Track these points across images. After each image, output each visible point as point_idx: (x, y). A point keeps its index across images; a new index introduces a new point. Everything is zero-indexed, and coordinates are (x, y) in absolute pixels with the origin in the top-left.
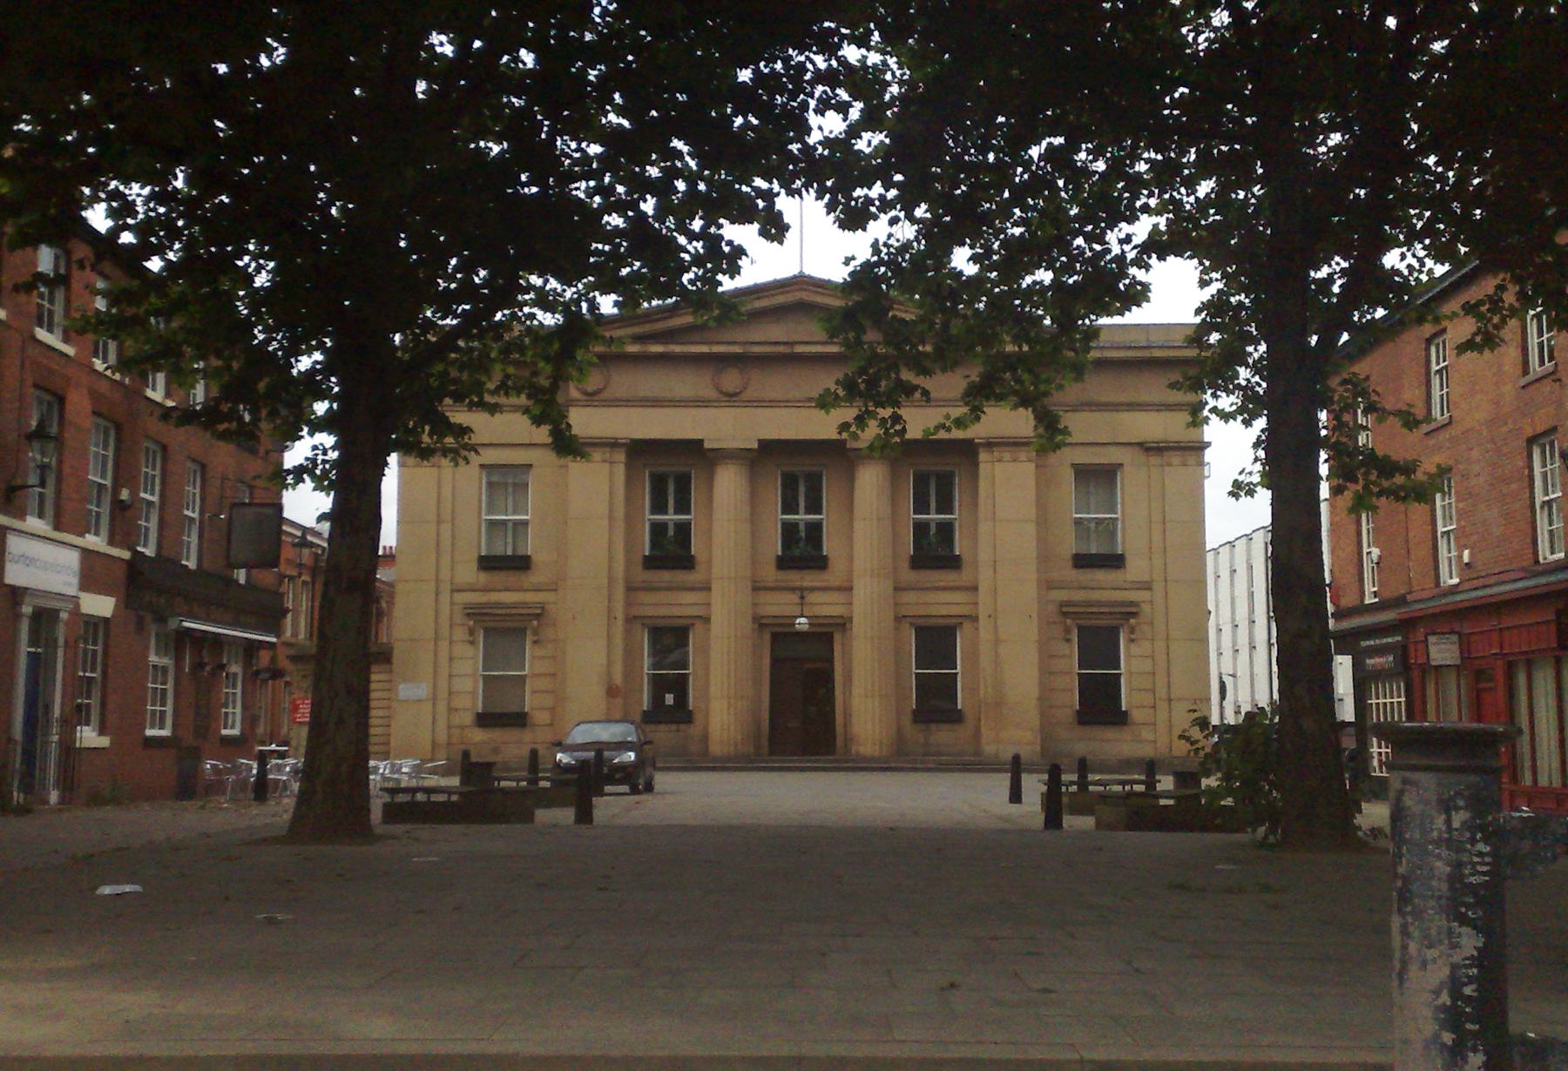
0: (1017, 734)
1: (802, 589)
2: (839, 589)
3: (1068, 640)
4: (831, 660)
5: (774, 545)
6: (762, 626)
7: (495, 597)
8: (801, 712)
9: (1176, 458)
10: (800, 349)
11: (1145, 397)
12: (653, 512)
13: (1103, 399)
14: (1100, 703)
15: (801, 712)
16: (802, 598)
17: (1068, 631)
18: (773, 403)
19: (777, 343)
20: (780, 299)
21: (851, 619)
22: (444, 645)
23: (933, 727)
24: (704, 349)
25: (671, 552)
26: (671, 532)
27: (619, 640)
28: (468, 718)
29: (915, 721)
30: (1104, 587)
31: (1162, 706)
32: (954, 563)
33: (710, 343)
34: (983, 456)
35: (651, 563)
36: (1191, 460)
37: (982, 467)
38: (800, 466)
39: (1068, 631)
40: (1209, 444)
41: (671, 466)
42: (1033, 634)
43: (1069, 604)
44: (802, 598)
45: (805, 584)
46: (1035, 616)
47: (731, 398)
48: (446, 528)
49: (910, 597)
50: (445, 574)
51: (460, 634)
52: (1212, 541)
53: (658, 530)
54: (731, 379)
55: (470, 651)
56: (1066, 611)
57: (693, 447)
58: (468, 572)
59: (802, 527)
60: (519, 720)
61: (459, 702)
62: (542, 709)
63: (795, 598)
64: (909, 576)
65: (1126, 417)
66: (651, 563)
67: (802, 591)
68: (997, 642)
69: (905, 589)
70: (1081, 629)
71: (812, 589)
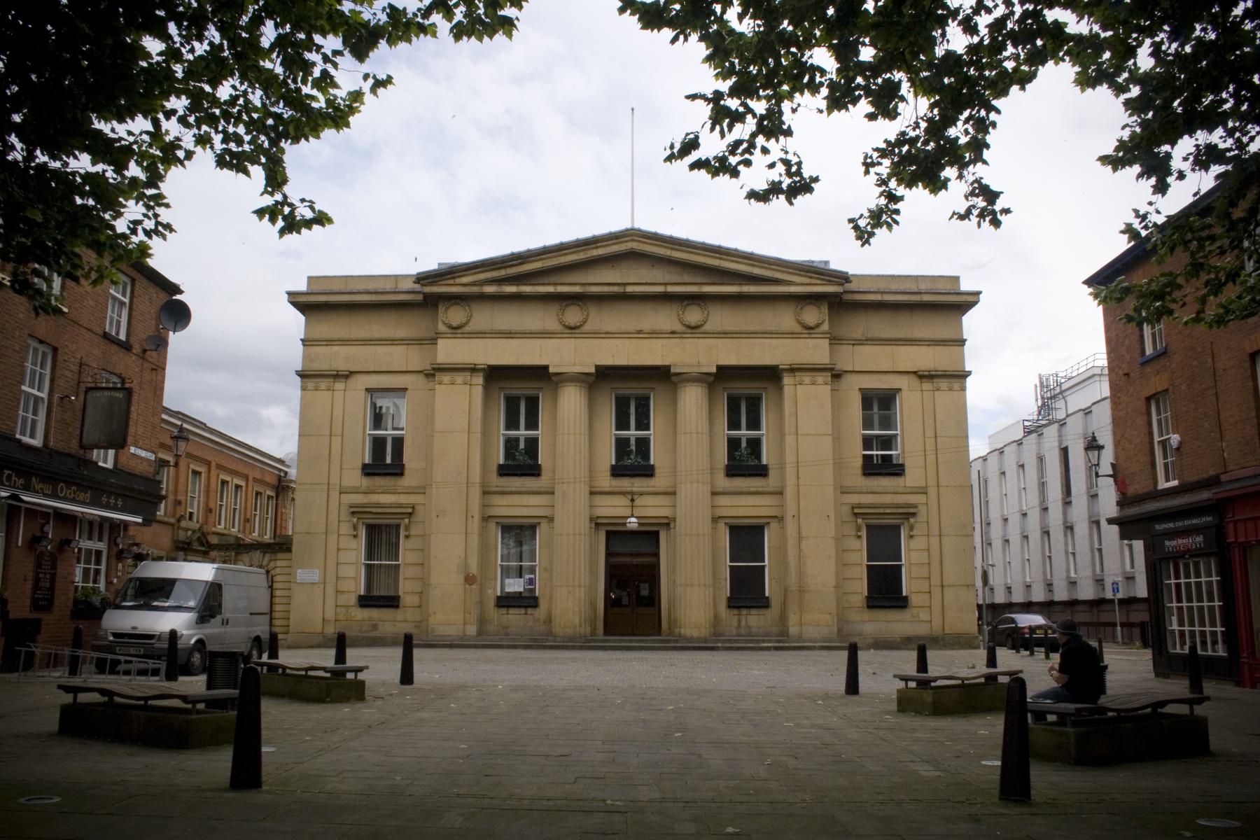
0: (815, 619)
1: (632, 493)
2: (665, 493)
3: (859, 537)
4: (657, 555)
5: (608, 456)
6: (597, 524)
7: (375, 498)
8: (632, 596)
9: (944, 384)
10: (630, 289)
11: (918, 333)
12: (617, 429)
13: (884, 336)
14: (885, 589)
15: (632, 596)
16: (632, 500)
17: (859, 529)
18: (608, 335)
19: (613, 284)
20: (616, 248)
21: (674, 519)
22: (333, 538)
23: (744, 612)
24: (550, 289)
25: (522, 463)
26: (522, 446)
27: (475, 540)
28: (353, 600)
29: (730, 607)
30: (884, 491)
31: (937, 592)
32: (762, 471)
33: (555, 284)
34: (787, 380)
35: (504, 471)
36: (956, 385)
37: (786, 388)
38: (632, 389)
39: (859, 529)
40: (969, 373)
41: (521, 389)
42: (832, 532)
43: (859, 506)
44: (632, 500)
45: (635, 489)
46: (832, 515)
47: (573, 330)
48: (336, 441)
49: (722, 501)
50: (335, 479)
51: (346, 529)
52: (973, 456)
53: (511, 444)
54: (573, 315)
55: (353, 543)
56: (857, 512)
57: (540, 373)
58: (354, 478)
59: (633, 441)
60: (392, 602)
61: (344, 586)
62: (413, 593)
63: (625, 501)
64: (723, 482)
65: (903, 350)
66: (504, 471)
67: (632, 496)
68: (800, 538)
69: (723, 493)
70: (869, 527)
71: (641, 494)
